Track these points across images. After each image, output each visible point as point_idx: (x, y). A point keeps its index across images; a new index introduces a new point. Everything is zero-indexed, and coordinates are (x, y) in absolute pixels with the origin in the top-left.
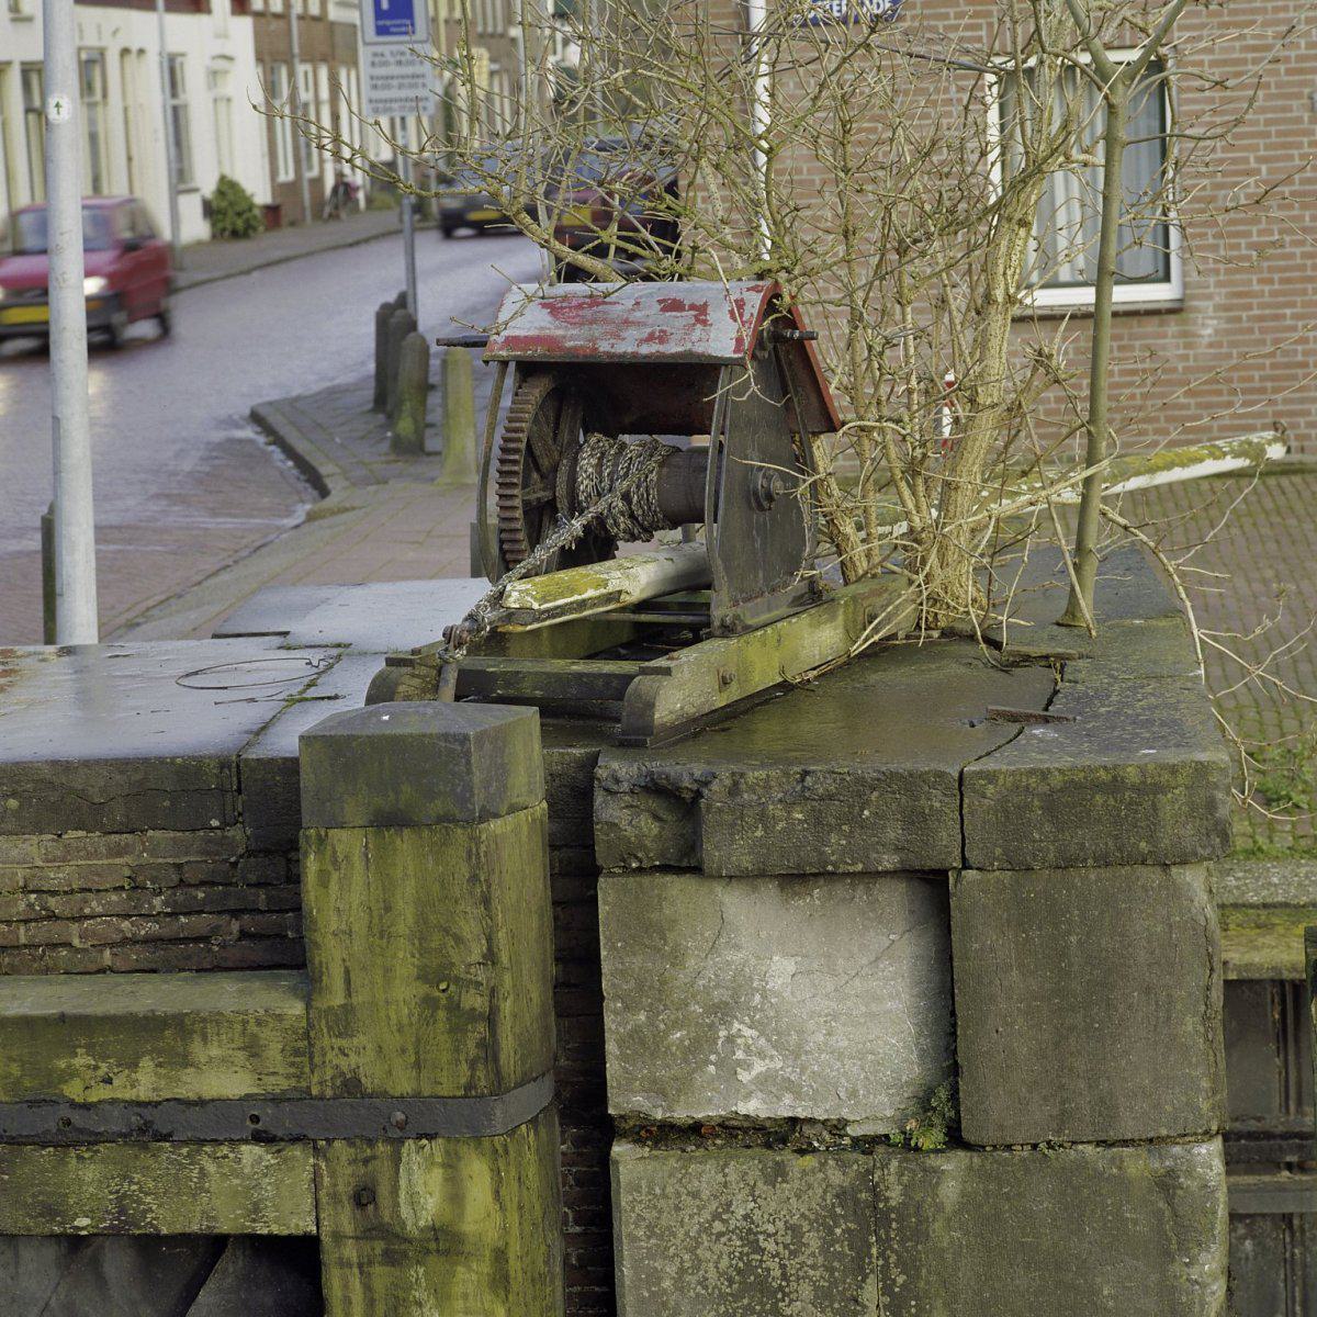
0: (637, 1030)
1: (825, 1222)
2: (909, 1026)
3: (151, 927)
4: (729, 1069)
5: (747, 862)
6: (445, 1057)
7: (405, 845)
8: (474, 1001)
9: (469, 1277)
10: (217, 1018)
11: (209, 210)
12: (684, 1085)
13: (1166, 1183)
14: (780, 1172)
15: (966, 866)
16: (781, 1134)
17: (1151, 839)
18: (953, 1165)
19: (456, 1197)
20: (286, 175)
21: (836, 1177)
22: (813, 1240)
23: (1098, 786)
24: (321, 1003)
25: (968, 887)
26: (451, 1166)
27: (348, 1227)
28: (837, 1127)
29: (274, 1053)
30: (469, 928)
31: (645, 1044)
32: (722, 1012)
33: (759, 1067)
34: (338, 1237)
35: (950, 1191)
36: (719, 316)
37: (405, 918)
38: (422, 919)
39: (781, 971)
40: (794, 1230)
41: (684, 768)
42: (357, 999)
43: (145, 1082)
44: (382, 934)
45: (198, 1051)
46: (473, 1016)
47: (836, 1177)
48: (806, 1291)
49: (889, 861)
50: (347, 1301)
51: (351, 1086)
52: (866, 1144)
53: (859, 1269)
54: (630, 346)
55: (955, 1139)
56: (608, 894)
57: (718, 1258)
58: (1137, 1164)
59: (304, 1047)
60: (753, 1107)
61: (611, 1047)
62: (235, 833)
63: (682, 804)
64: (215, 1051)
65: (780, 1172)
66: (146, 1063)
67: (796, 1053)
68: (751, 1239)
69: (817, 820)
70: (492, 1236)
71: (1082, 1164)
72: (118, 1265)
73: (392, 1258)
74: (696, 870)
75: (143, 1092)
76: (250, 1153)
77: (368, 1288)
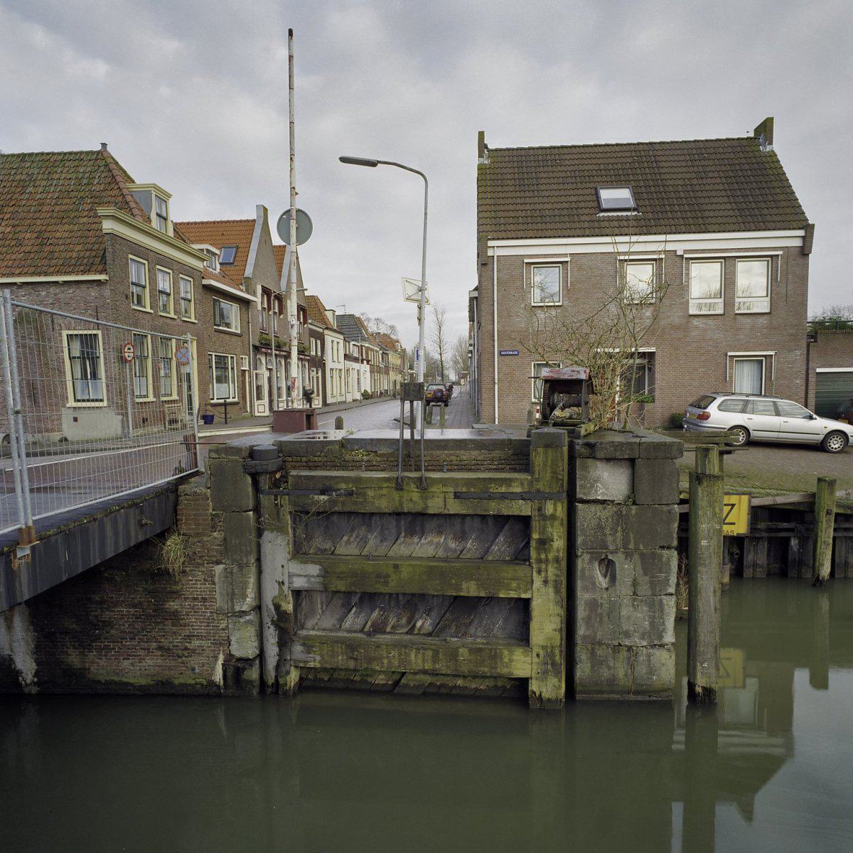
0: (582, 484)
1: (612, 516)
2: (626, 485)
3: (495, 467)
4: (596, 491)
5: (603, 456)
6: (555, 487)
7: (550, 451)
8: (560, 477)
9: (557, 523)
10: (517, 479)
11: (363, 395)
12: (589, 494)
13: (670, 512)
14: (605, 508)
15: (639, 458)
16: (603, 502)
17: (671, 454)
18: (634, 507)
19: (555, 510)
20: (373, 391)
21: (615, 509)
22: (610, 520)
23: (662, 445)
24: (534, 477)
25: (638, 462)
26: (555, 504)
27: (537, 514)
28: (613, 501)
29: (526, 485)
30: (560, 465)
31: (583, 487)
32: (596, 481)
33: (601, 491)
34: (535, 516)
35: (633, 512)
36: (582, 373)
37: (549, 462)
38: (552, 463)
39: (606, 475)
40: (607, 518)
41: (592, 440)
42: (541, 476)
43: (503, 489)
44: (545, 465)
45: (513, 485)
46: (560, 479)
47: (615, 509)
48: (609, 528)
49: (627, 457)
50: (536, 527)
51: (538, 491)
52: (619, 504)
53: (617, 524)
54: (566, 377)
55: (634, 503)
56: (578, 462)
57: (594, 522)
58: (665, 508)
59: (530, 484)
60: (599, 498)
61: (578, 487)
62: (510, 451)
63: (590, 446)
64: (515, 484)
65: (605, 508)
66: (504, 486)
67: (607, 489)
68: (600, 519)
69: (615, 450)
70: (561, 517)
71: (656, 508)
72: (490, 521)
73: (544, 520)
74: (594, 458)
75: (503, 491)
76: (521, 501)
77: (539, 524)
